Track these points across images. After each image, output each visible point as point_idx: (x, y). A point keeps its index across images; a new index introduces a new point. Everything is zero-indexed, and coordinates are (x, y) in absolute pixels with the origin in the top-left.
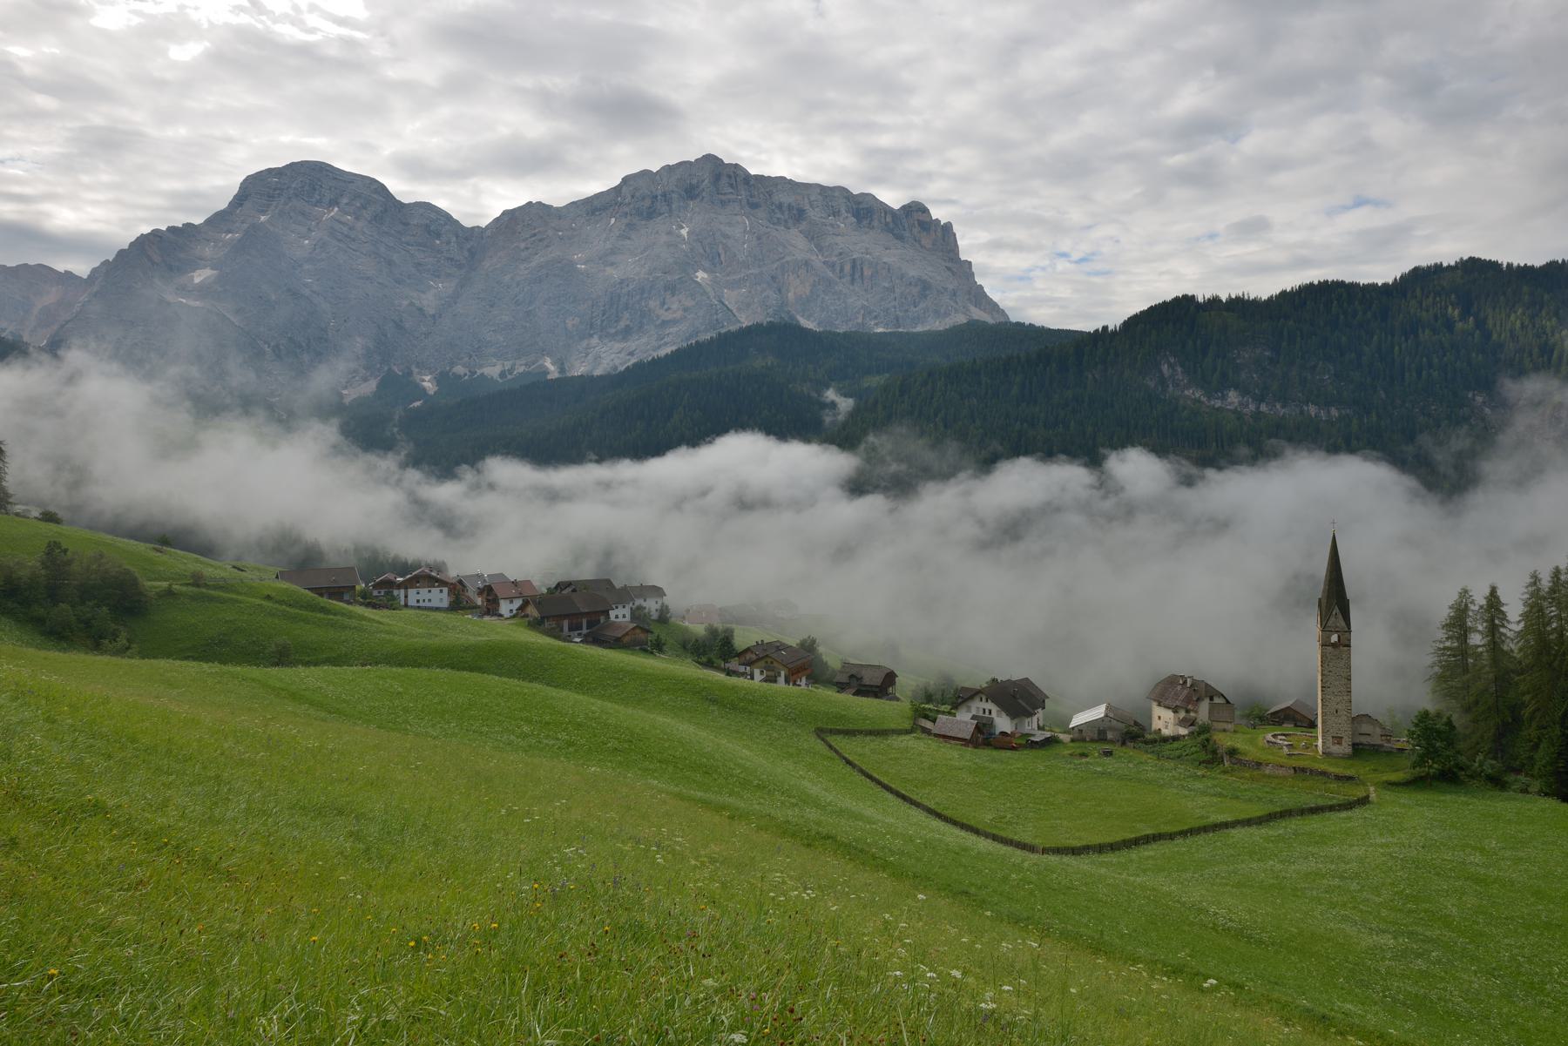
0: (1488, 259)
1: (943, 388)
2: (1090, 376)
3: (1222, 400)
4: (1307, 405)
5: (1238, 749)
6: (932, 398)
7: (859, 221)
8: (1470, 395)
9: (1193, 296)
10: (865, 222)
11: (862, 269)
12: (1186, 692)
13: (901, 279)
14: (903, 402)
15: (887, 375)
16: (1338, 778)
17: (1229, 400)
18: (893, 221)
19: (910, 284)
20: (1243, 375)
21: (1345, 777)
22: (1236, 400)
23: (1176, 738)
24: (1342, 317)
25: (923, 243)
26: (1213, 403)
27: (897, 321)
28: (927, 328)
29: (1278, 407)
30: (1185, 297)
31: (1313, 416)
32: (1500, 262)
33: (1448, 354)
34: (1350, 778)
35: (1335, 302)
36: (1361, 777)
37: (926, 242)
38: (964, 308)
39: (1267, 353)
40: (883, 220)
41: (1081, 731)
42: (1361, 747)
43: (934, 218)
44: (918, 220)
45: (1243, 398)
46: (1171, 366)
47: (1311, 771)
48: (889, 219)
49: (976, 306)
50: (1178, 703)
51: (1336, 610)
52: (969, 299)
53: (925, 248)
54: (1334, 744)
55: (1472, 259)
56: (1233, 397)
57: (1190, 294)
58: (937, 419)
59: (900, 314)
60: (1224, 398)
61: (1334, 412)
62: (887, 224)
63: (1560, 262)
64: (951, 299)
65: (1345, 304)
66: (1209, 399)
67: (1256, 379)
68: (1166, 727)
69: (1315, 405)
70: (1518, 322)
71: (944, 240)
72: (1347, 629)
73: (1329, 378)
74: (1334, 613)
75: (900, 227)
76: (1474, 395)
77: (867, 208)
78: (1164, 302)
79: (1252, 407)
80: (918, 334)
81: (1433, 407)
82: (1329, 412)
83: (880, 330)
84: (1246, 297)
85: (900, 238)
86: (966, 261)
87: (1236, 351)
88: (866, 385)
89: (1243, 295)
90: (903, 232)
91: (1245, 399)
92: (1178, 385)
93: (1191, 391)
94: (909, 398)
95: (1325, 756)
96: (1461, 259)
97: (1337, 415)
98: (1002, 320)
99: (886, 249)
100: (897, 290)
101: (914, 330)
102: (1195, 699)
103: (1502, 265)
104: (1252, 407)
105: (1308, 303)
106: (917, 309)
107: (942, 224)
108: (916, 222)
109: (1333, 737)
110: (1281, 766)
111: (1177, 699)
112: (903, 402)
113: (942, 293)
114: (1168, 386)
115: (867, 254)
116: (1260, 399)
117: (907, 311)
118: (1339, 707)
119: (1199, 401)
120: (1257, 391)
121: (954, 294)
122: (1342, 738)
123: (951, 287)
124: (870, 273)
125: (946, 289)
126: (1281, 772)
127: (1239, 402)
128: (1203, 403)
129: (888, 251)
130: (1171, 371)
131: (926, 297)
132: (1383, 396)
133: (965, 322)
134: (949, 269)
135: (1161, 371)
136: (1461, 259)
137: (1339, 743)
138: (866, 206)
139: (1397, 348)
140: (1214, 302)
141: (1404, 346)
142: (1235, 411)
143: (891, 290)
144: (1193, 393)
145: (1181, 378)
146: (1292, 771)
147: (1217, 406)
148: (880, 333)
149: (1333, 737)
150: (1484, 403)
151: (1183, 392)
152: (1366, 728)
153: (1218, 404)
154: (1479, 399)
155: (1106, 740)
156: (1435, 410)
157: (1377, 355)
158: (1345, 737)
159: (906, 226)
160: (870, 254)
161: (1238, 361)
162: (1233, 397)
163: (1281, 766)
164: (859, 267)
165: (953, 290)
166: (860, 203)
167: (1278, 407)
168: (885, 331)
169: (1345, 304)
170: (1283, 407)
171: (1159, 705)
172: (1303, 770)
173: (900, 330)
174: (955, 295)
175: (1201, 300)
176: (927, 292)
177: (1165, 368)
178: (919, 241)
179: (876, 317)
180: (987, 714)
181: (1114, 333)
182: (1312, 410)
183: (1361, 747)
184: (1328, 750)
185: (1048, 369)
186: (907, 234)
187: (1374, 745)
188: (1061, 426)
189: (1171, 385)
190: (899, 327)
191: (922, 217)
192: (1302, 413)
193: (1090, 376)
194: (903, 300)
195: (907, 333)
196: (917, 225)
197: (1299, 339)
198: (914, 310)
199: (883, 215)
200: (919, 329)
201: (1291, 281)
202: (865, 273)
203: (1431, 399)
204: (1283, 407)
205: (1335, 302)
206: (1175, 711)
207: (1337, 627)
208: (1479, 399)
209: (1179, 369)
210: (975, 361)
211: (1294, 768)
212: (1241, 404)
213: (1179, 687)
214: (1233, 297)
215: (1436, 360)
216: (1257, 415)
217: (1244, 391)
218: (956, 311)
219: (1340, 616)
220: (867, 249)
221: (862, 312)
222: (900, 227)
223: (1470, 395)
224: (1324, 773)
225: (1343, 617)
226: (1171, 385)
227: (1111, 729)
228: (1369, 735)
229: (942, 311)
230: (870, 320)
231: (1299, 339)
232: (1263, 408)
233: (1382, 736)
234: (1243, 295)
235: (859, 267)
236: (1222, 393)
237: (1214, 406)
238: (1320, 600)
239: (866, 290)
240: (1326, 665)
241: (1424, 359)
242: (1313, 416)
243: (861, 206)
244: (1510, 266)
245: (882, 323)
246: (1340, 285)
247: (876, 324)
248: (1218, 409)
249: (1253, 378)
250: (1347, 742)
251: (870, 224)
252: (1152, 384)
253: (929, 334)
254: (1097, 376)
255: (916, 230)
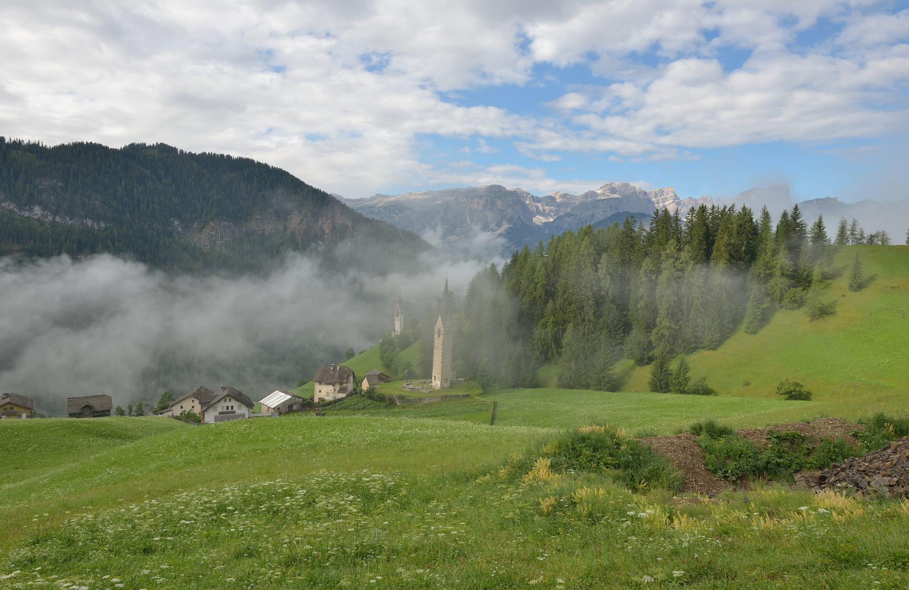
3: (29, 212)
4: (86, 219)
8: (172, 220)
16: (464, 396)
17: (35, 212)
20: (44, 196)
22: (39, 213)
23: (336, 401)
24: (103, 167)
26: (23, 213)
29: (67, 219)
31: (90, 226)
33: (162, 196)
34: (468, 396)
35: (99, 157)
39: (59, 184)
41: (279, 408)
45: (44, 211)
47: (450, 396)
55: (162, 144)
56: (37, 211)
60: (31, 210)
61: (102, 224)
65: (104, 159)
66: (20, 211)
67: (53, 200)
68: (328, 396)
69: (91, 219)
70: (193, 183)
73: (99, 204)
76: (174, 220)
79: (50, 218)
81: (155, 225)
82: (99, 224)
84: (40, 145)
89: (39, 143)
91: (46, 212)
93: (7, 204)
96: (157, 143)
97: (104, 226)
104: (50, 218)
105: (82, 155)
111: (334, 379)
116: (56, 213)
119: (11, 211)
120: (53, 208)
127: (41, 214)
128: (15, 212)
132: (129, 217)
139: (135, 190)
141: (139, 188)
142: (38, 220)
144: (8, 206)
147: (25, 216)
150: (178, 224)
153: (27, 214)
154: (176, 222)
155: (292, 411)
156: (156, 227)
157: (125, 193)
161: (41, 187)
162: (37, 211)
167: (67, 219)
169: (104, 159)
170: (71, 219)
171: (320, 383)
172: (446, 397)
180: (230, 409)
182: (89, 222)
192: (82, 223)
197: (80, 176)
201: (68, 139)
203: (154, 221)
204: (71, 219)
205: (99, 157)
208: (176, 222)
212: (42, 215)
213: (332, 372)
215: (156, 199)
216: (54, 224)
217: (45, 207)
223: (172, 220)
224: (457, 396)
227: (295, 403)
232: (58, 219)
236: (29, 207)
237: (23, 215)
241: (150, 198)
242: (90, 226)
244: (181, 151)
246: (81, 145)
248: (27, 217)
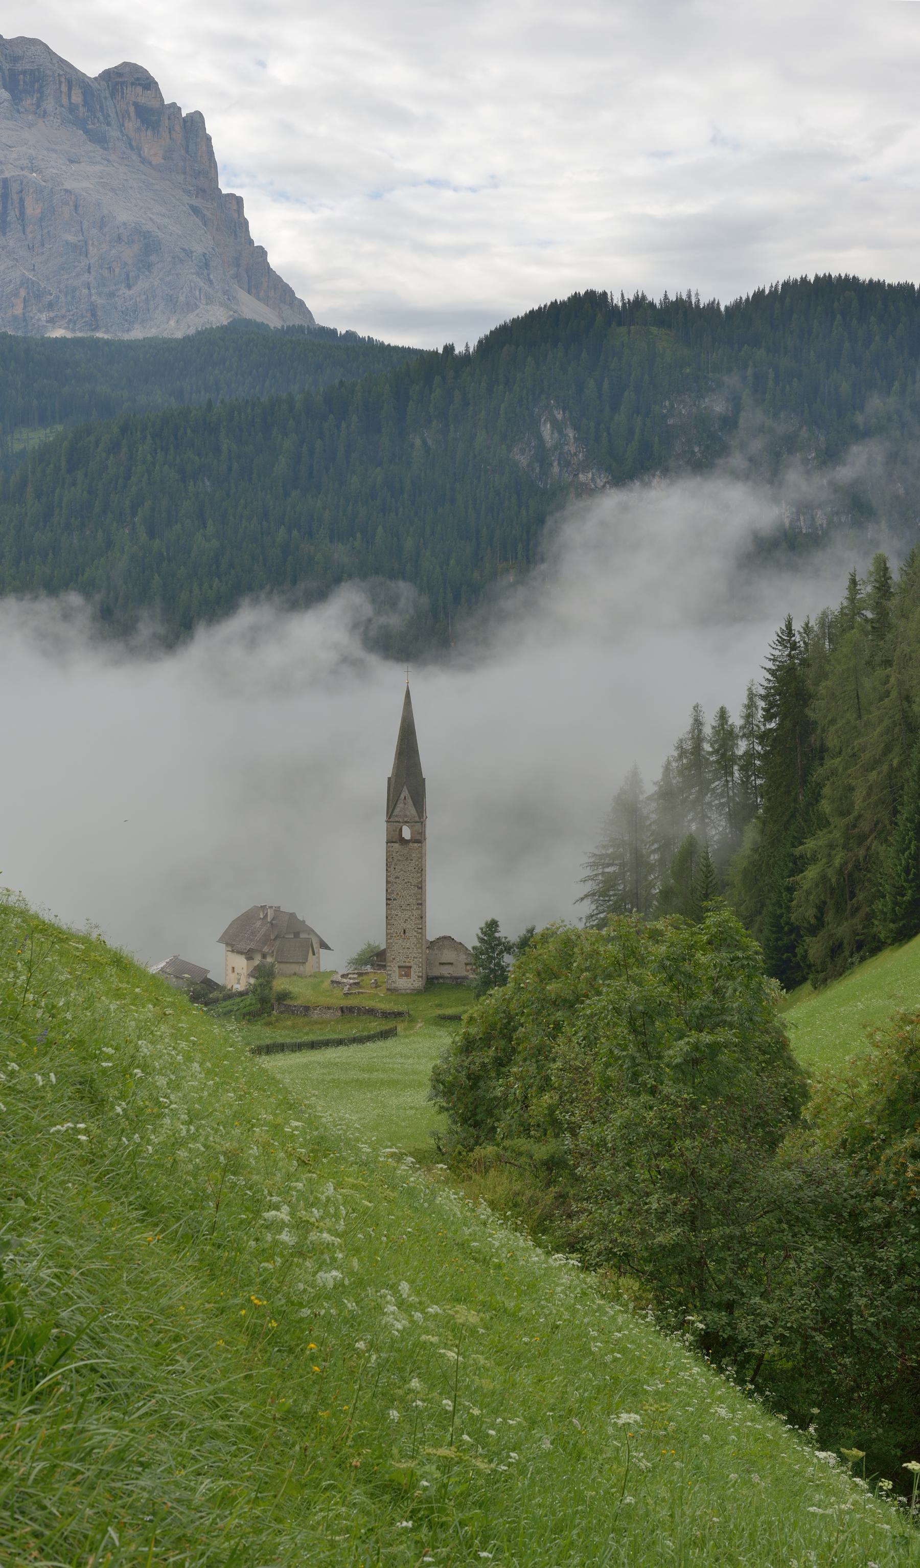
0: (386, 343)
1: (149, 458)
2: (418, 442)
5: (290, 993)
6: (128, 478)
7: (16, 98)
9: (605, 294)
10: (29, 102)
11: (22, 201)
12: (264, 929)
13: (101, 228)
14: (74, 484)
15: (60, 428)
18: (85, 101)
19: (119, 238)
21: (394, 1013)
24: (847, 345)
25: (146, 152)
27: (94, 315)
28: (152, 332)
30: (590, 294)
32: (881, 281)
35: (839, 317)
36: (411, 1012)
37: (153, 149)
38: (225, 294)
40: (65, 101)
42: (441, 981)
43: (167, 102)
44: (136, 105)
46: (558, 427)
47: (359, 1009)
48: (77, 98)
49: (249, 292)
50: (252, 945)
51: (405, 793)
52: (236, 276)
53: (150, 163)
54: (401, 976)
57: (599, 290)
58: (136, 519)
59: (99, 301)
62: (72, 109)
63: (440, 351)
64: (197, 274)
68: (239, 983)
71: (187, 152)
72: (417, 819)
74: (402, 796)
75: (99, 115)
77: (32, 72)
78: (554, 304)
80: (130, 346)
83: (58, 333)
84: (694, 300)
85: (99, 139)
86: (233, 195)
87: (667, 403)
88: (18, 447)
89: (689, 296)
90: (105, 127)
92: (568, 464)
93: (590, 475)
94: (86, 475)
95: (389, 993)
98: (297, 321)
99: (71, 161)
100: (92, 250)
101: (126, 337)
102: (272, 937)
103: (912, 285)
106: (131, 292)
107: (184, 115)
108: (132, 109)
109: (399, 967)
110: (329, 1008)
112: (74, 484)
113: (182, 261)
114: (551, 465)
115: (33, 171)
117: (111, 295)
118: (407, 926)
121: (205, 264)
122: (410, 967)
123: (199, 249)
124: (38, 211)
125: (189, 253)
126: (328, 1016)
129: (74, 167)
130: (556, 435)
131: (149, 266)
133: (225, 323)
134: (195, 210)
135: (540, 438)
136: (830, 276)
137: (408, 975)
138: (28, 67)
140: (639, 304)
143: (80, 250)
145: (573, 450)
146: (339, 1013)
148: (63, 341)
149: (399, 967)
151: (576, 475)
152: (448, 955)
158: (414, 967)
159: (112, 114)
160: (39, 171)
161: (670, 422)
163: (329, 1008)
164: (15, 197)
165: (204, 255)
166: (16, 59)
168: (69, 335)
172: (351, 1010)
173: (99, 335)
174: (207, 266)
175: (617, 301)
176: (153, 258)
177: (546, 430)
178: (139, 150)
179: (50, 306)
181: (466, 358)
183: (441, 981)
184: (393, 985)
185: (344, 425)
186: (114, 133)
187: (456, 978)
188: (359, 535)
189: (556, 464)
190: (96, 329)
191: (144, 99)
193: (418, 442)
194: (106, 273)
195: (107, 343)
196: (133, 114)
197: (771, 383)
198: (129, 293)
199: (64, 88)
200: (137, 334)
202: (29, 211)
206: (250, 958)
207: (406, 816)
209: (571, 433)
210: (210, 404)
211: (342, 1009)
214: (672, 298)
218: (209, 300)
219: (410, 801)
220: (31, 159)
221: (23, 293)
222: (99, 115)
225: (414, 805)
226: (556, 464)
228: (452, 964)
229: (182, 298)
230: (40, 311)
231: (771, 383)
233: (467, 964)
234: (689, 296)
235: (15, 197)
238: (389, 779)
239: (31, 248)
240: (392, 869)
243: (19, 67)
245: (63, 317)
247: (52, 321)
249: (693, 453)
250: (415, 972)
251: (38, 106)
252: (523, 460)
253: (150, 344)
254: (430, 442)
255: (132, 125)
